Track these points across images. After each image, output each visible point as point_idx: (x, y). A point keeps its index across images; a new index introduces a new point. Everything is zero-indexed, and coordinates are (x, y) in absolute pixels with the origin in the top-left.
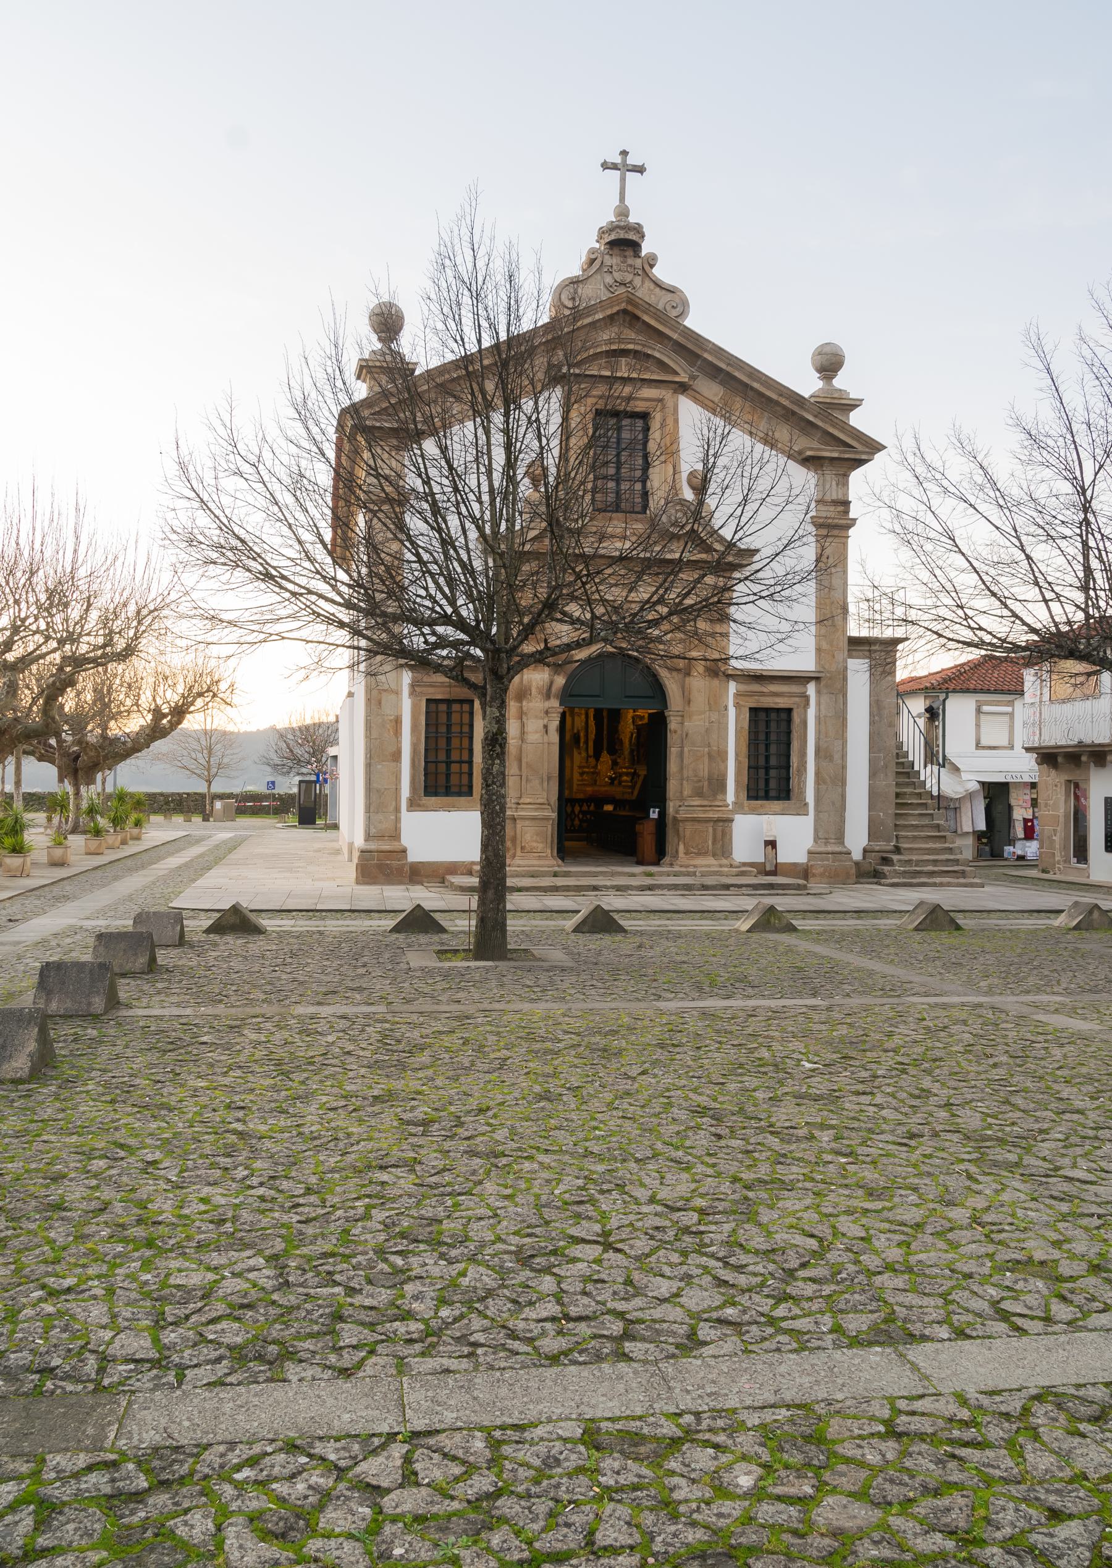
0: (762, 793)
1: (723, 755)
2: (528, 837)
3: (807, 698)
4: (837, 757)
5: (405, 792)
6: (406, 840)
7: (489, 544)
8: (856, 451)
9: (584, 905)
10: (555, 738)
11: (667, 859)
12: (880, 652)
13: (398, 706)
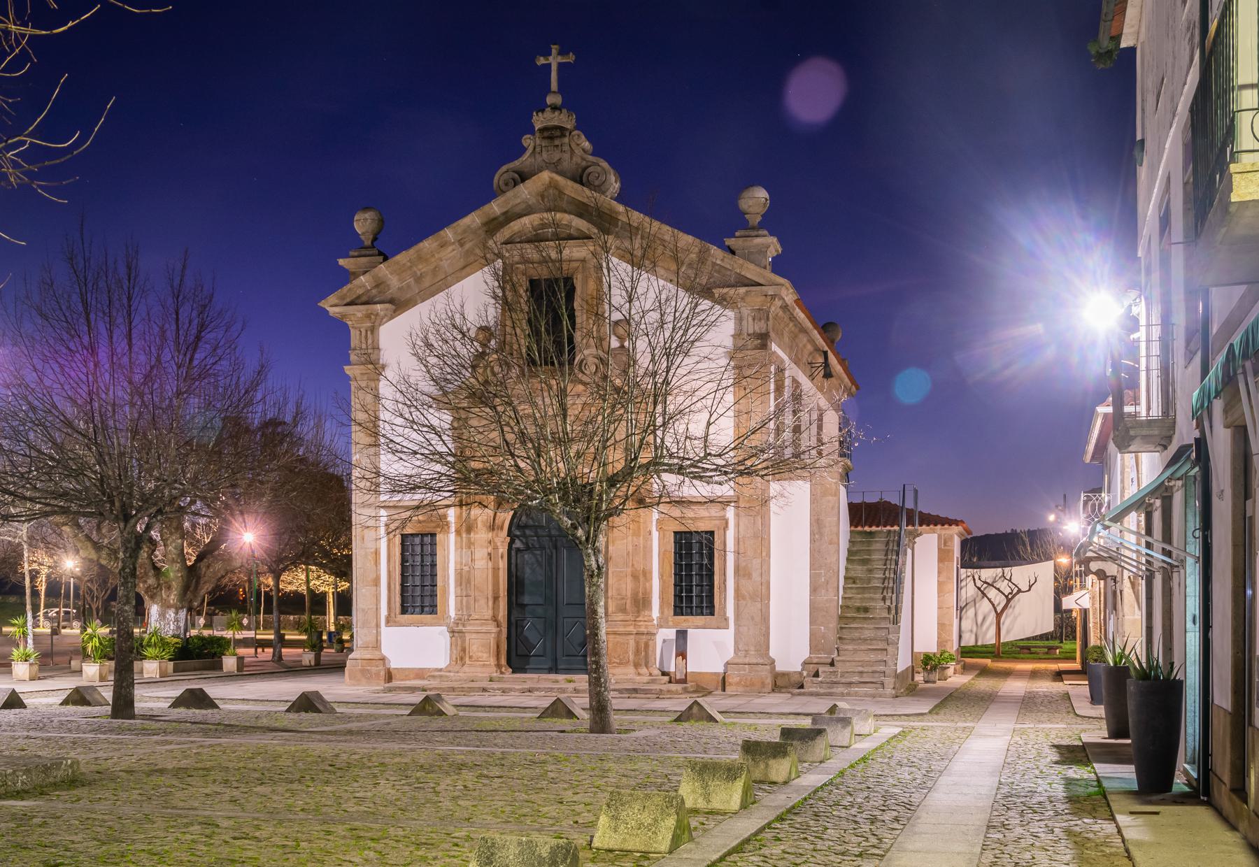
1: (647, 574)
2: (474, 648)
4: (756, 576)
6: (385, 651)
7: (84, 616)
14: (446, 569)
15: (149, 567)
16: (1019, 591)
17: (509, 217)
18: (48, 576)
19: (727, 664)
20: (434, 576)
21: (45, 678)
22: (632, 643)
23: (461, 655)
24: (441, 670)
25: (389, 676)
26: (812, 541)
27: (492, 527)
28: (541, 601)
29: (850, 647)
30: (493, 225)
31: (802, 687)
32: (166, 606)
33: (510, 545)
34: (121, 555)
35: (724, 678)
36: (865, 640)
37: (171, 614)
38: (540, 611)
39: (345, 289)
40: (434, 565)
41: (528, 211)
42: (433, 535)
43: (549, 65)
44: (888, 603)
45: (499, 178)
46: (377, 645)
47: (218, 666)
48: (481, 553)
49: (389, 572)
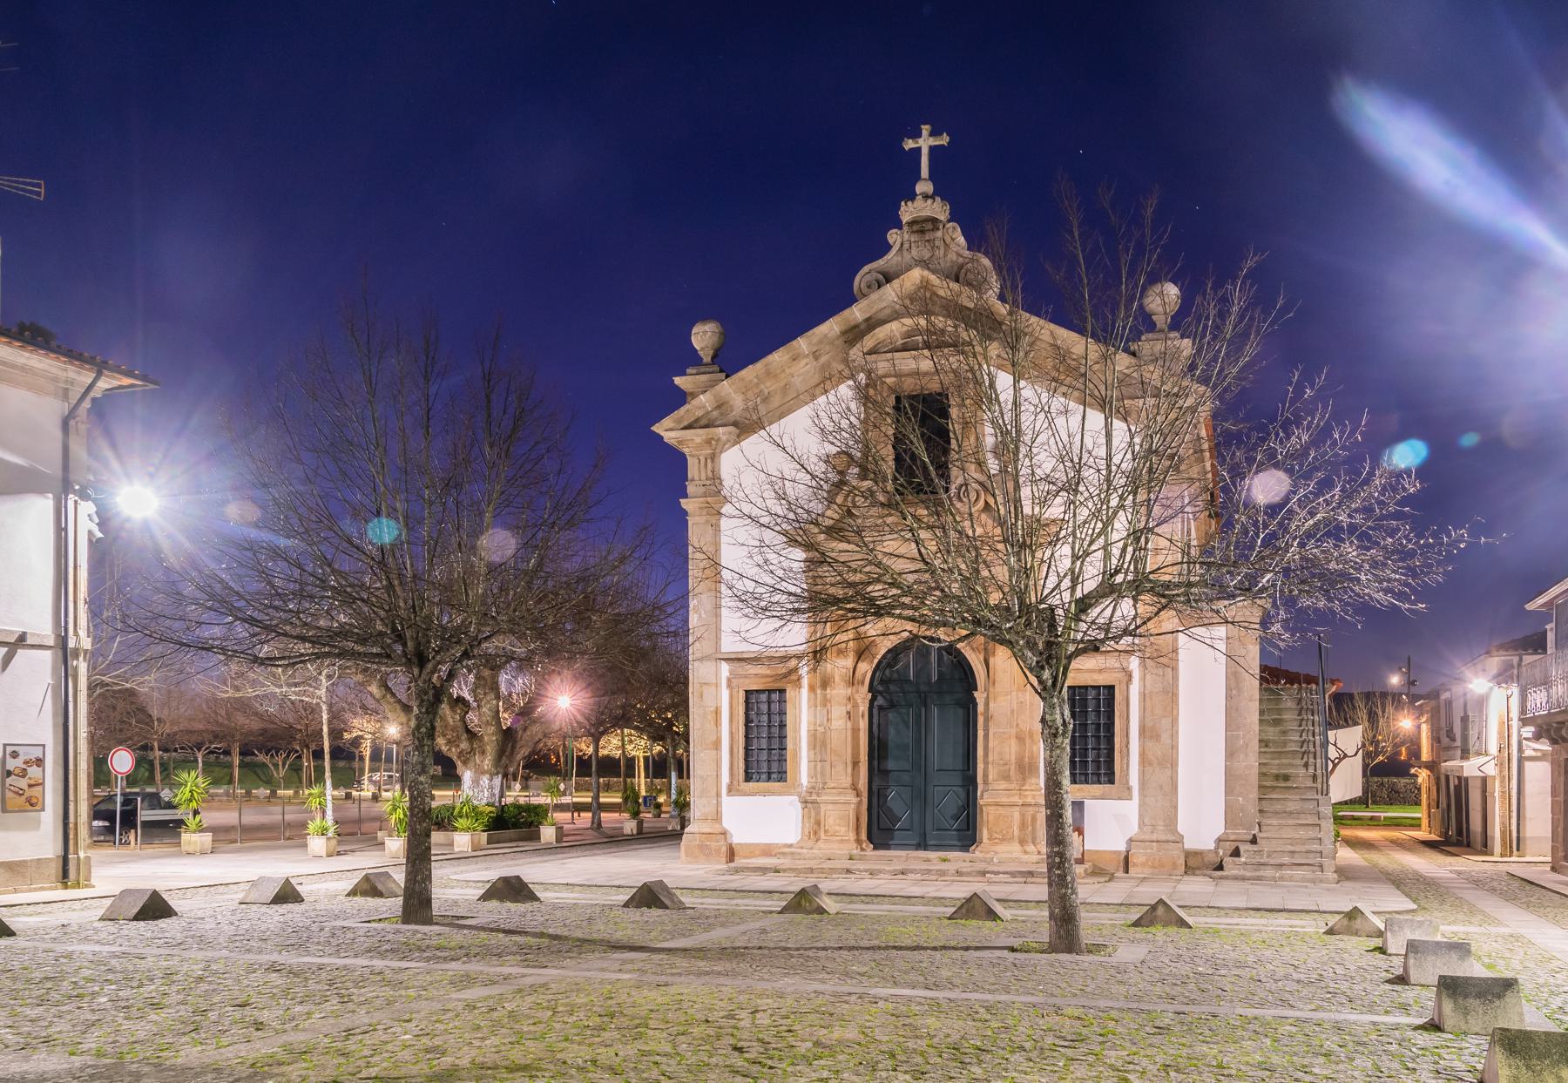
2: (830, 821)
3: (1130, 676)
4: (1165, 738)
5: (725, 779)
6: (727, 823)
9: (961, 891)
13: (718, 697)
14: (797, 730)
15: (461, 730)
16: (1346, 756)
17: (872, 324)
18: (373, 741)
19: (1131, 840)
20: (783, 737)
21: (345, 853)
22: (1017, 815)
23: (815, 829)
24: (791, 846)
25: (731, 854)
26: (1229, 697)
27: (852, 681)
28: (908, 767)
29: (1275, 822)
30: (854, 334)
31: (1220, 867)
32: (480, 771)
33: (872, 702)
34: (416, 710)
35: (1126, 859)
36: (1291, 813)
37: (485, 780)
38: (906, 777)
39: (683, 410)
40: (782, 726)
41: (895, 316)
42: (782, 691)
43: (919, 149)
44: (1311, 770)
45: (860, 279)
46: (718, 818)
47: (535, 837)
48: (838, 712)
49: (731, 733)
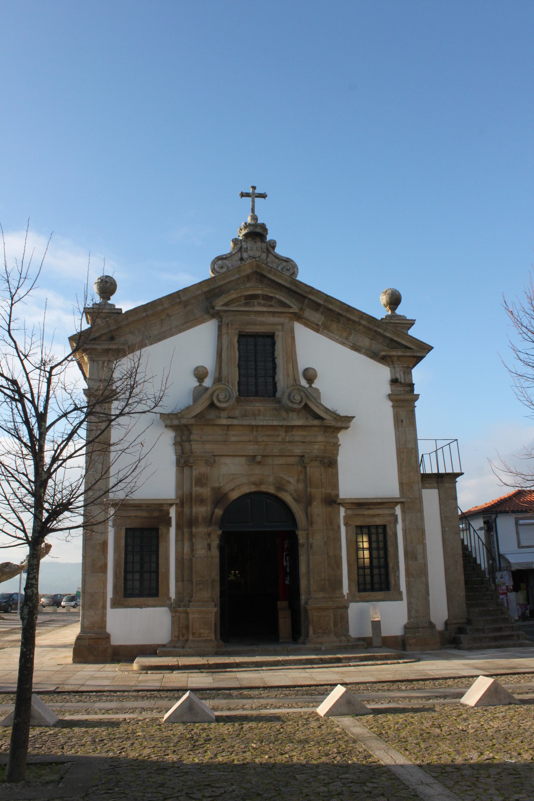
0: (368, 587)
3: (396, 517)
4: (420, 557)
5: (110, 594)
6: (110, 629)
8: (418, 351)
10: (215, 553)
11: (302, 638)
12: (445, 482)
42: (157, 530)
